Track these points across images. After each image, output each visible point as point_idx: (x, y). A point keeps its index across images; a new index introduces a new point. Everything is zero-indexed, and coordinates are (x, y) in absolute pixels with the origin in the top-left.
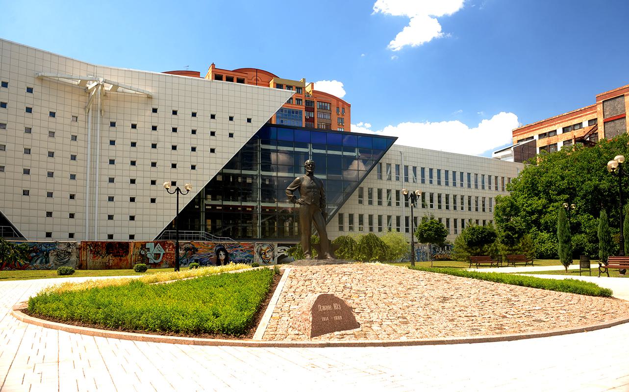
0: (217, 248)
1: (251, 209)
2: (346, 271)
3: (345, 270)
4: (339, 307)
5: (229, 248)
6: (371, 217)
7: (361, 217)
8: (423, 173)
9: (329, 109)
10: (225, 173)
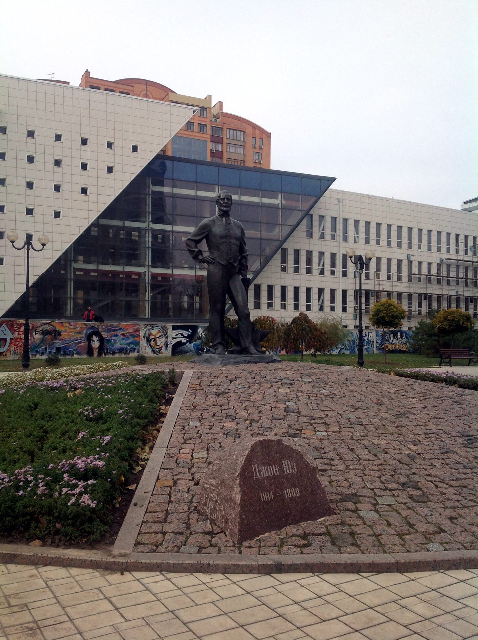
0: (89, 332)
1: (137, 277)
2: (282, 377)
3: (282, 374)
4: (293, 467)
5: (105, 331)
6: (296, 290)
7: (284, 289)
8: (370, 230)
9: (242, 139)
10: (102, 225)
